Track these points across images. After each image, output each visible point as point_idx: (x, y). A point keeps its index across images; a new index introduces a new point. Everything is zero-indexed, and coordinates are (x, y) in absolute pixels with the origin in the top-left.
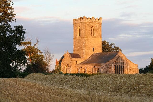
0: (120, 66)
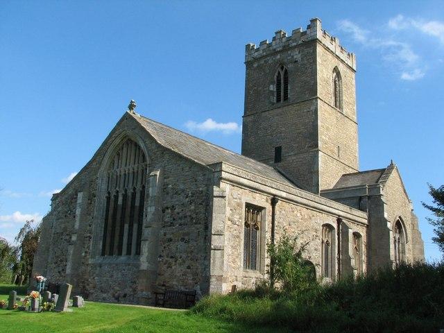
0: (125, 196)
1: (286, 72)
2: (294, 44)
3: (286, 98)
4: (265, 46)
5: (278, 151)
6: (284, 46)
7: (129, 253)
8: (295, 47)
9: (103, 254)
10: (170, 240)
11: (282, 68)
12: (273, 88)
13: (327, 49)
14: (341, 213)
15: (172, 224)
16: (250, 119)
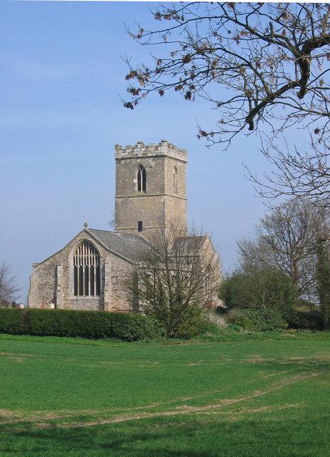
1: (144, 171)
2: (151, 155)
3: (144, 189)
4: (130, 150)
5: (140, 224)
6: (143, 154)
7: (92, 294)
8: (151, 157)
9: (76, 294)
12: (136, 181)
16: (120, 200)
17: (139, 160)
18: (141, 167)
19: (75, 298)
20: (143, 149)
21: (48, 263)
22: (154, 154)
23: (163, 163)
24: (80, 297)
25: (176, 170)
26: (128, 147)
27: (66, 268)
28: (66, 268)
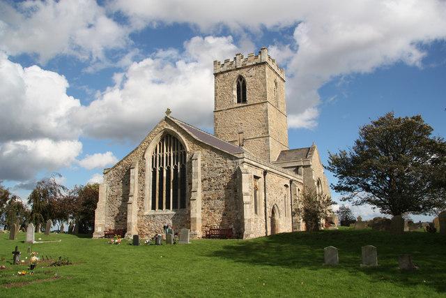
3: (245, 101)
4: (229, 64)
7: (168, 207)
9: (154, 208)
10: (209, 199)
11: (241, 80)
13: (271, 68)
14: (292, 178)
15: (209, 189)
17: (238, 72)
18: (240, 78)
19: (153, 212)
20: (242, 60)
21: (120, 167)
22: (254, 63)
23: (264, 72)
24: (158, 212)
25: (276, 84)
26: (227, 61)
27: (142, 172)
28: (142, 172)
